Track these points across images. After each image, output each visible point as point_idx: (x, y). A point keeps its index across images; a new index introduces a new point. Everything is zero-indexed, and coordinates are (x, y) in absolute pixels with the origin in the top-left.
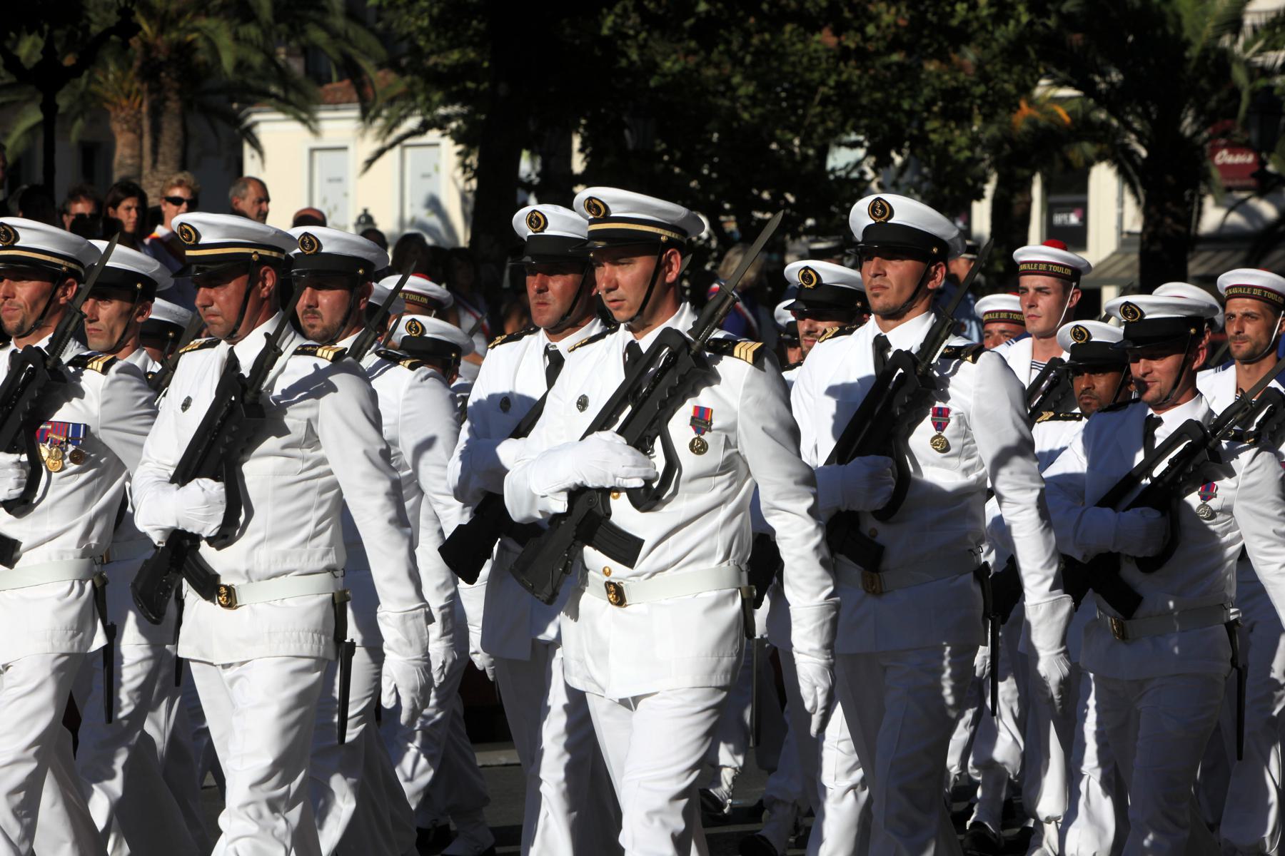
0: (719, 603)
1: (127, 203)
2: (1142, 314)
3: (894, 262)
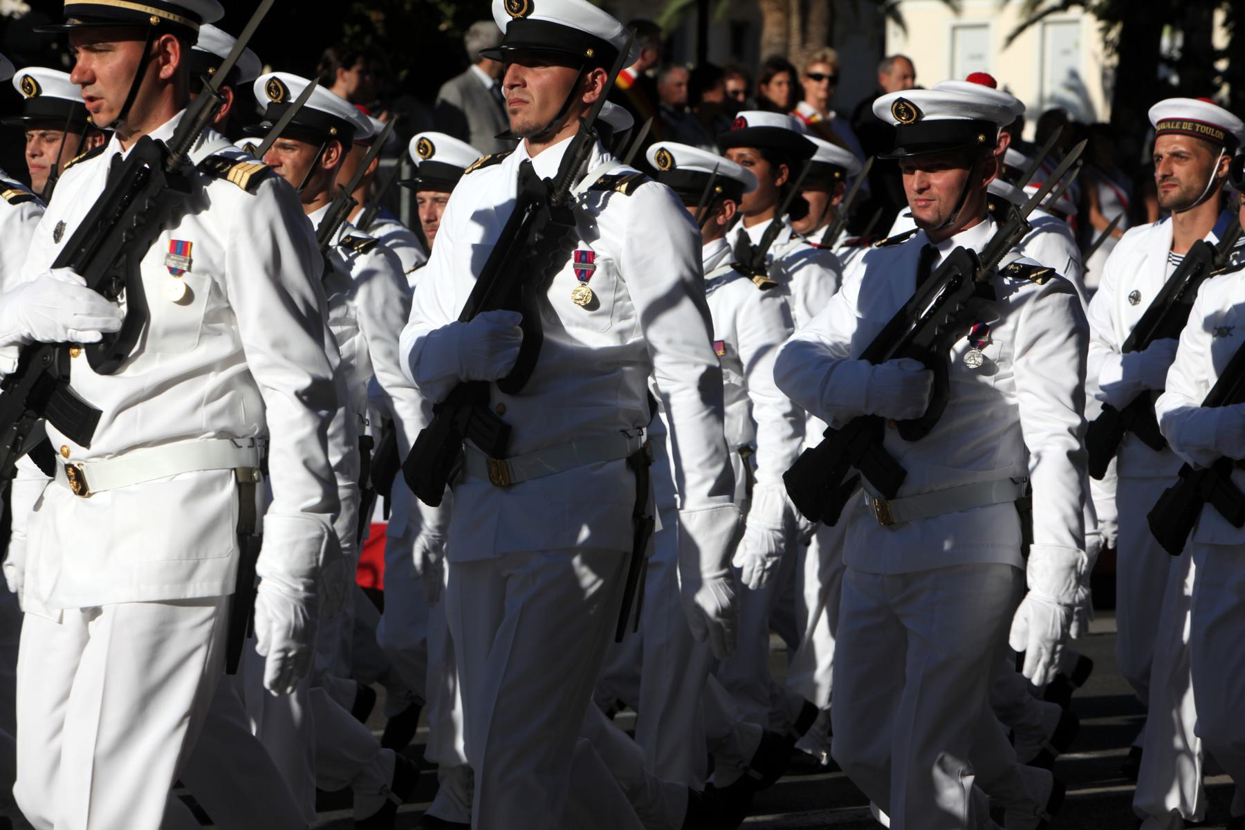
0: (201, 490)
1: (779, 77)
2: (39, 89)
3: (536, 69)
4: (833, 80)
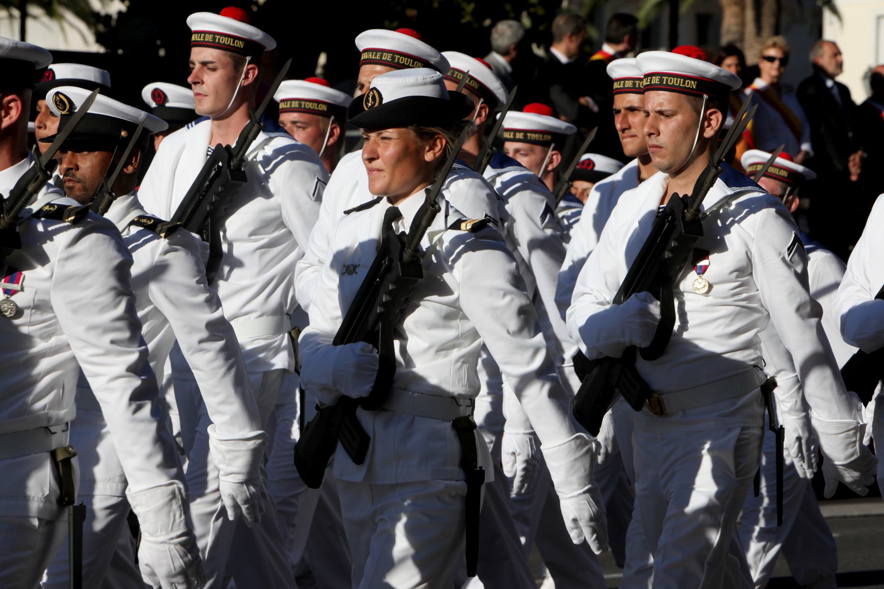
4: (784, 62)
